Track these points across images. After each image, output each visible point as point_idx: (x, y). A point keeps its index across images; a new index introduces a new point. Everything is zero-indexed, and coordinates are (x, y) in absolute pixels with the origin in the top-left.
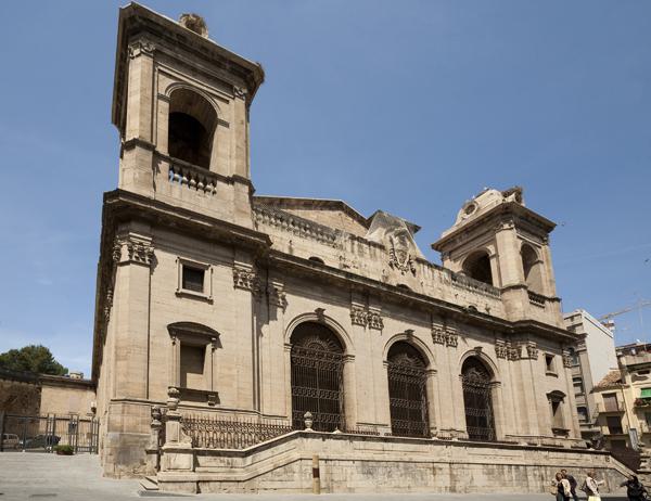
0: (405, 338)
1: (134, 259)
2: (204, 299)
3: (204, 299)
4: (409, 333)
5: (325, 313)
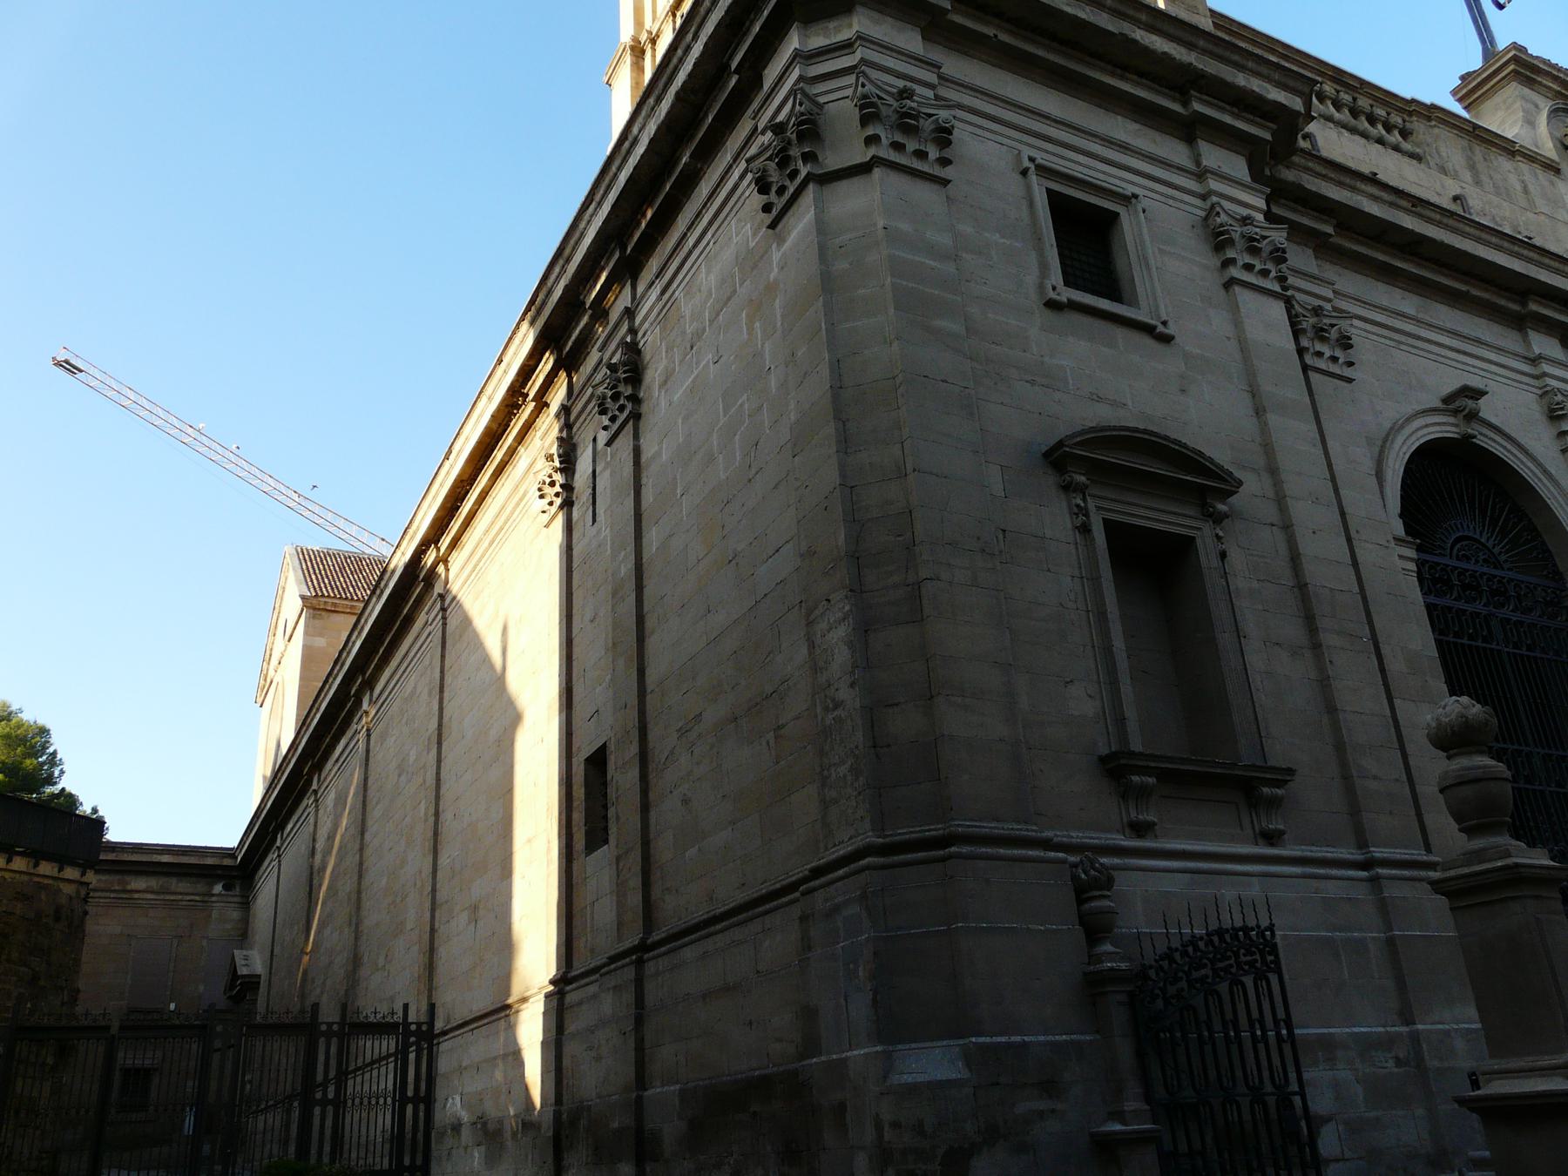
0: (1444, 428)
2: (1148, 329)
3: (1148, 329)
4: (1463, 401)
5: (1486, 408)
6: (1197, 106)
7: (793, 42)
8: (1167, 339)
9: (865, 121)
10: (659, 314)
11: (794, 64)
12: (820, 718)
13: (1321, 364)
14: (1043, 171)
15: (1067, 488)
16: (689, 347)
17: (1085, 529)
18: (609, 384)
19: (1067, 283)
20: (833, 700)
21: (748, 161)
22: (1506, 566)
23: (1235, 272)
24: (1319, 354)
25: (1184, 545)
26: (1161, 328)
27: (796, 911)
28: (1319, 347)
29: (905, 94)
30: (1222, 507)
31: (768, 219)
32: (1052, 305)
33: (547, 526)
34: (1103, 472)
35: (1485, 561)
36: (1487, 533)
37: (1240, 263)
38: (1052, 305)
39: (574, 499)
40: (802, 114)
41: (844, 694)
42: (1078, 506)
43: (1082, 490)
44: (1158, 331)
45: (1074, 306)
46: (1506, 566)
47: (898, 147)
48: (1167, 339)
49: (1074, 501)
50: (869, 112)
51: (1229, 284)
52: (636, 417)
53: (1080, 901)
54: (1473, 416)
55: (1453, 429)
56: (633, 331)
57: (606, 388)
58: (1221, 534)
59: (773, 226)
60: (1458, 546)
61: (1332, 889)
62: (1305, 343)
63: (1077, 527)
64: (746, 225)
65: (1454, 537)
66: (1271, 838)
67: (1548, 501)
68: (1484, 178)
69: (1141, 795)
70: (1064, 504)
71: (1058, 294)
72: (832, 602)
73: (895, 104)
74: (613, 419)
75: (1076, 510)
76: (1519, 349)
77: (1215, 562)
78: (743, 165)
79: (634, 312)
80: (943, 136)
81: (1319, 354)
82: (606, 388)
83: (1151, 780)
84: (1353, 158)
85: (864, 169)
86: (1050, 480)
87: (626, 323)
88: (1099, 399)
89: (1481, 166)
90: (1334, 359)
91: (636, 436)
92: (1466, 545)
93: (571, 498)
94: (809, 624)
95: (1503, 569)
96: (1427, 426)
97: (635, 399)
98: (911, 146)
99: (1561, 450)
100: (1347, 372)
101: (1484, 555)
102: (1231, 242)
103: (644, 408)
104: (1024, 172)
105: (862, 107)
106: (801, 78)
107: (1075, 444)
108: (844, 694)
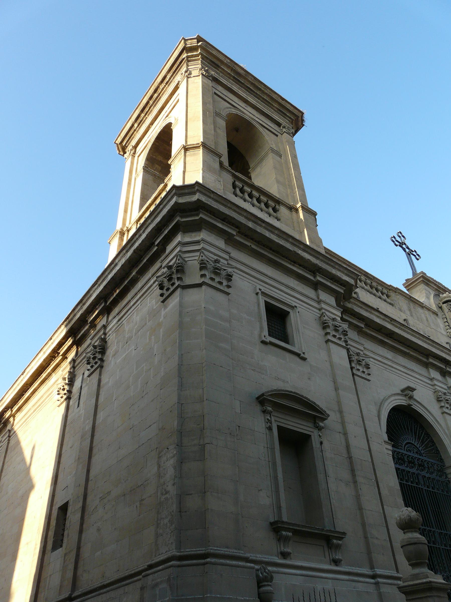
0: (401, 401)
1: (207, 281)
2: (298, 355)
3: (298, 355)
6: (319, 278)
7: (179, 238)
8: (304, 359)
9: (201, 269)
10: (116, 329)
11: (178, 246)
12: (159, 497)
13: (359, 373)
14: (264, 294)
15: (264, 412)
16: (125, 343)
17: (270, 429)
18: (92, 353)
19: (270, 335)
20: (165, 490)
21: (157, 277)
22: (424, 455)
23: (330, 337)
24: (358, 370)
25: (307, 438)
26: (302, 355)
27: (139, 585)
28: (358, 367)
29: (216, 261)
30: (321, 424)
31: (162, 299)
32: (263, 342)
33: (59, 406)
34: (278, 407)
35: (416, 452)
36: (417, 442)
37: (331, 334)
38: (263, 342)
39: (72, 396)
40: (179, 263)
41: (170, 487)
42: (268, 419)
43: (270, 413)
44: (301, 356)
45: (271, 344)
46: (424, 455)
47: (212, 279)
48: (304, 359)
49: (266, 417)
50: (203, 265)
51: (327, 341)
52: (101, 367)
53: (259, 587)
54: (411, 398)
55: (405, 402)
56: (105, 334)
57: (91, 354)
58: (321, 435)
59: (163, 302)
60: (407, 446)
61: (361, 587)
62: (353, 365)
63: (267, 428)
64: (153, 300)
65: (405, 442)
66: (336, 562)
67: (438, 432)
68: (414, 314)
69: (286, 540)
70: (263, 418)
71: (266, 339)
72: (169, 449)
73: (213, 264)
74: (92, 367)
75: (267, 421)
76: (426, 375)
77: (318, 445)
78: (155, 278)
79: (106, 327)
80: (229, 277)
81: (358, 370)
82: (91, 354)
83: (290, 534)
84: (371, 302)
85: (199, 286)
86: (258, 408)
87: (103, 330)
88: (278, 379)
89: (413, 310)
90: (363, 372)
91: (100, 374)
92: (410, 446)
93: (70, 396)
94: (159, 457)
95: (423, 456)
96: (396, 400)
97: (102, 360)
98: (217, 279)
99: (442, 413)
100: (368, 377)
101: (416, 450)
102: (328, 326)
103: (105, 364)
104: (257, 294)
105: (201, 264)
106: (180, 251)
107: (268, 395)
108: (170, 487)
